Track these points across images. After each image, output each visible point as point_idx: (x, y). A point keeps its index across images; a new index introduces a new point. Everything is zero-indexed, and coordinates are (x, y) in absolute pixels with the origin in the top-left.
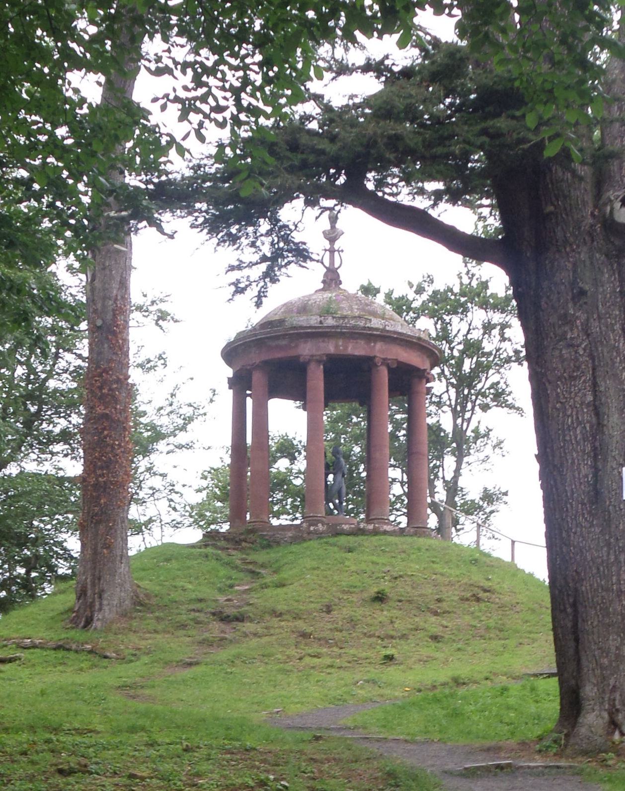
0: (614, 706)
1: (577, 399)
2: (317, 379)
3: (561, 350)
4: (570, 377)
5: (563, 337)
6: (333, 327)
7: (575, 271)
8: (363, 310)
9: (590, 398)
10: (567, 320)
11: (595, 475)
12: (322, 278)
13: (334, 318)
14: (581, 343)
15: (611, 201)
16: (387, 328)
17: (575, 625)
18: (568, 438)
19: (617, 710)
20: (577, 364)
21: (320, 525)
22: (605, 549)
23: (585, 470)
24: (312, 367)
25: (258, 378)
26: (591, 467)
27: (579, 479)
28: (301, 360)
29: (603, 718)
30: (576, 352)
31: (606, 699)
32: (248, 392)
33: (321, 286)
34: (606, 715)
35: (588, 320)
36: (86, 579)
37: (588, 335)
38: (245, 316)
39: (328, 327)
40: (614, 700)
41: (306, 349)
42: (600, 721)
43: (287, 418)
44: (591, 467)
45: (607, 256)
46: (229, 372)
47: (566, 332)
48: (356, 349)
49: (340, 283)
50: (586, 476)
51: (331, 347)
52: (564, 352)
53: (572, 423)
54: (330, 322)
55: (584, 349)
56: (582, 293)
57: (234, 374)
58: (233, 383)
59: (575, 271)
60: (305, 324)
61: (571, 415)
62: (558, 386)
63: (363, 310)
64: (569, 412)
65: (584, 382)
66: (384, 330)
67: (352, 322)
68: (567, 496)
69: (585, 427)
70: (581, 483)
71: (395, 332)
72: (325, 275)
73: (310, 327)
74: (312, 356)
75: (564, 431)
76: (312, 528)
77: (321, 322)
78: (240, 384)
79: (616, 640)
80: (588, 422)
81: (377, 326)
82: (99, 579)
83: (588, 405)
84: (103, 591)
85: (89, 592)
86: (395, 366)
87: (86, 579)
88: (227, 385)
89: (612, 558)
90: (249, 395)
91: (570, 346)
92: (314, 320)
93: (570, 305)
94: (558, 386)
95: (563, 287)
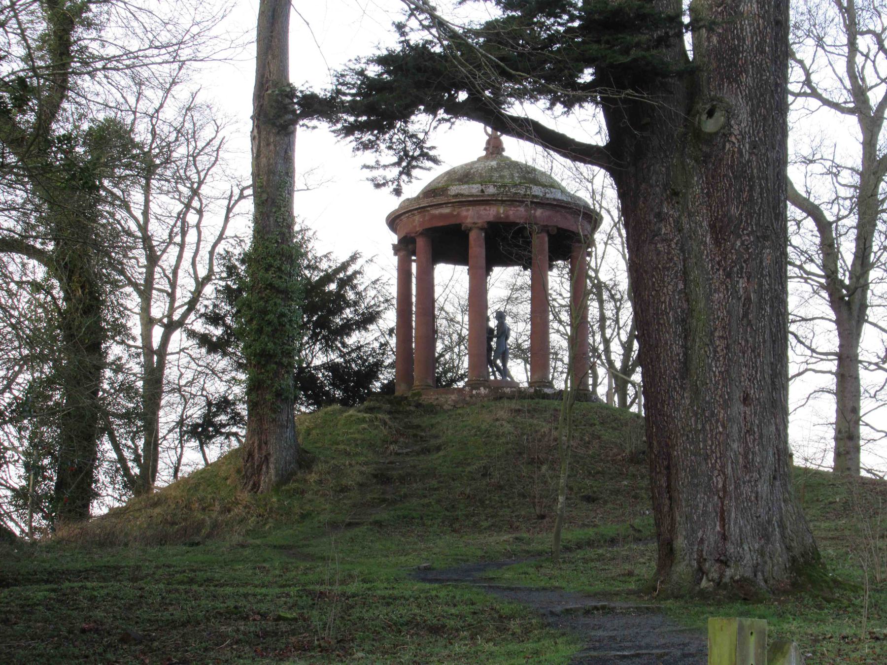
0: (701, 556)
1: (670, 287)
2: (477, 245)
3: (656, 244)
4: (664, 268)
5: (657, 233)
6: (493, 195)
7: (668, 175)
8: (525, 178)
9: (681, 286)
10: (661, 217)
11: (685, 354)
12: (484, 146)
13: (495, 186)
14: (673, 238)
15: (698, 112)
16: (547, 196)
17: (668, 486)
18: (662, 322)
19: (705, 560)
20: (670, 256)
21: (482, 389)
22: (693, 419)
23: (676, 349)
24: (473, 235)
25: (421, 243)
26: (682, 346)
27: (671, 357)
28: (463, 228)
29: (692, 567)
30: (669, 246)
31: (695, 550)
32: (414, 258)
33: (484, 153)
34: (695, 564)
35: (680, 217)
36: (253, 443)
37: (680, 231)
38: (394, 204)
39: (488, 195)
40: (702, 551)
41: (470, 216)
42: (689, 568)
43: (451, 281)
44: (682, 346)
45: (696, 161)
46: (394, 239)
47: (660, 229)
48: (517, 214)
49: (503, 150)
50: (678, 355)
51: (491, 213)
52: (659, 246)
53: (666, 308)
54: (491, 190)
55: (676, 244)
56: (676, 194)
57: (400, 241)
58: (397, 249)
59: (668, 175)
60: (466, 192)
61: (665, 302)
62: (653, 276)
63: (525, 178)
64: (662, 299)
65: (676, 272)
66: (544, 197)
67: (513, 190)
68: (660, 372)
69: (677, 313)
70: (673, 361)
71: (554, 199)
72: (488, 142)
73: (472, 196)
74: (475, 223)
75: (657, 315)
76: (474, 392)
77: (482, 191)
78: (405, 248)
79: (703, 498)
80: (679, 307)
81: (537, 193)
82: (266, 443)
83: (680, 292)
84: (269, 454)
85: (257, 456)
86: (555, 233)
87: (253, 443)
88: (393, 252)
89: (700, 427)
90: (414, 261)
91: (663, 240)
92: (475, 189)
93: (665, 204)
94: (653, 276)
95: (658, 189)
